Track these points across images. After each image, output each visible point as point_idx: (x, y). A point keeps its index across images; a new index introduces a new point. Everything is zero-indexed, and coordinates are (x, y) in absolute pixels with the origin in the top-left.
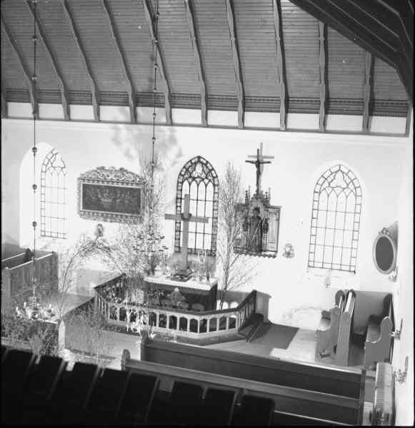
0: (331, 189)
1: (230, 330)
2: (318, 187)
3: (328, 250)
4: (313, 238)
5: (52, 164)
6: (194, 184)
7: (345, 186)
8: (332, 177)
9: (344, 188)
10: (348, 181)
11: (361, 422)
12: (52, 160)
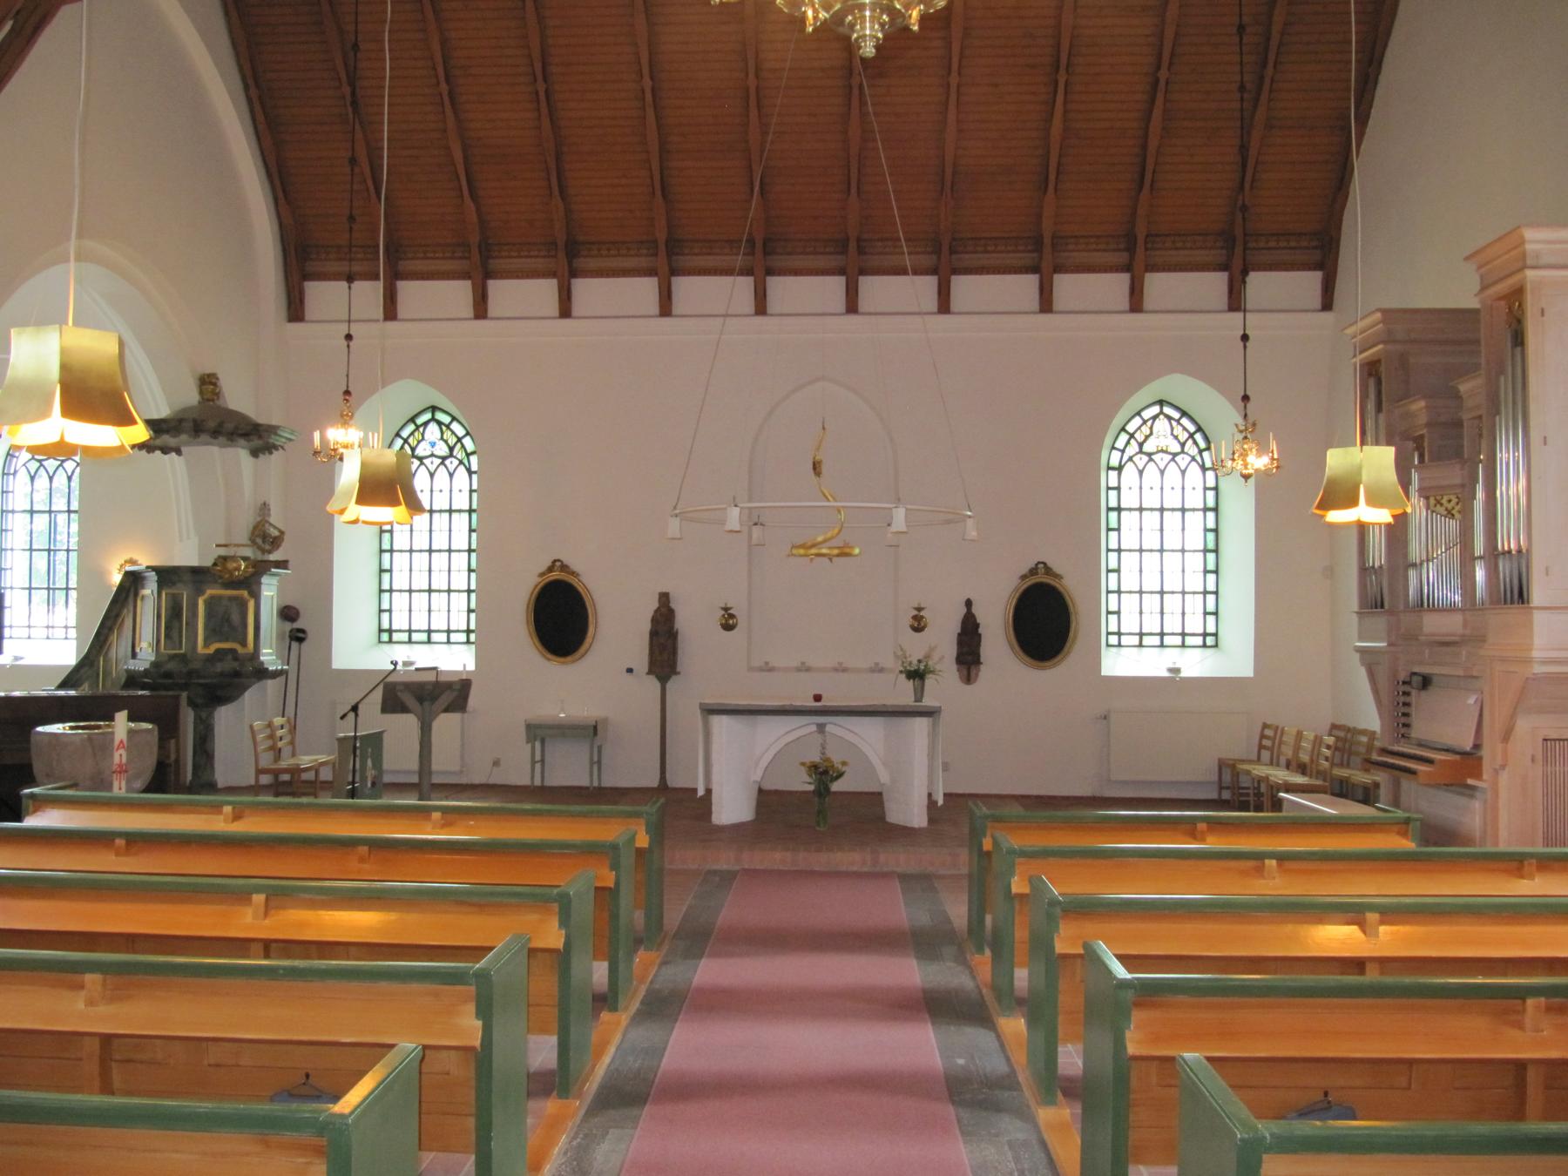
0: (1145, 458)
1: (1485, 777)
3: (1151, 602)
4: (435, 637)
7: (1176, 448)
8: (1145, 429)
10: (452, 441)
11: (1496, 844)
12: (1140, 437)
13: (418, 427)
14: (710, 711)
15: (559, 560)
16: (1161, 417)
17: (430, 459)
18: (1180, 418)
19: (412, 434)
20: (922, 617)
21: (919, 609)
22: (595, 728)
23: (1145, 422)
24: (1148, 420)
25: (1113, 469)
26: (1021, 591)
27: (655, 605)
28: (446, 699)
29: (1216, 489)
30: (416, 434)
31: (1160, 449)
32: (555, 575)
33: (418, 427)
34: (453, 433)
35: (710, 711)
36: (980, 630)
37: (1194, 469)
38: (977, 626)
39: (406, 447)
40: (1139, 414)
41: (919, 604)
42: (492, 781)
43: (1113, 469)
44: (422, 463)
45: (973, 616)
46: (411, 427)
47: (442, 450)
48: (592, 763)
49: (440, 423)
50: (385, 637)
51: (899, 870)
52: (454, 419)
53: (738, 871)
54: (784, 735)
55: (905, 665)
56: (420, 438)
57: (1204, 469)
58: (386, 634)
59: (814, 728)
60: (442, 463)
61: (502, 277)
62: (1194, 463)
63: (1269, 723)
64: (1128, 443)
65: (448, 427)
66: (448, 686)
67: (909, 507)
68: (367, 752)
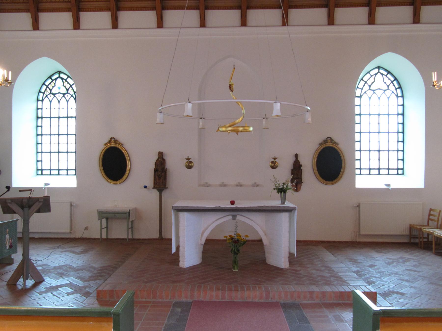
0: (52, 96)
2: (41, 95)
3: (375, 155)
4: (61, 172)
5: (51, 90)
6: (55, 101)
7: (65, 91)
8: (372, 80)
9: (385, 91)
12: (369, 83)
13: (53, 80)
14: (179, 210)
15: (113, 138)
16: (379, 74)
18: (387, 74)
19: (50, 83)
20: (276, 162)
21: (275, 159)
22: (129, 213)
26: (320, 150)
27: (157, 158)
28: (36, 206)
29: (403, 105)
30: (52, 83)
32: (113, 145)
33: (53, 80)
34: (68, 83)
35: (179, 210)
36: (302, 168)
37: (394, 97)
38: (301, 166)
39: (48, 89)
40: (369, 72)
41: (274, 156)
42: (84, 236)
44: (55, 96)
45: (299, 162)
46: (50, 81)
47: (64, 91)
48: (128, 229)
49: (62, 79)
50: (40, 172)
51: (282, 301)
52: (68, 77)
53: (192, 302)
54: (216, 221)
55: (276, 185)
57: (397, 96)
58: (40, 171)
59: (230, 217)
60: (64, 96)
61: (86, 11)
62: (393, 94)
63: (433, 208)
65: (66, 80)
66: (37, 200)
67: (282, 103)
68: (6, 231)
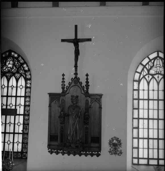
0: (151, 77)
17: (157, 75)
19: (148, 63)
23: (150, 60)
24: (152, 60)
25: (136, 81)
31: (157, 72)
39: (145, 69)
43: (136, 81)
56: (152, 65)
64: (143, 70)
